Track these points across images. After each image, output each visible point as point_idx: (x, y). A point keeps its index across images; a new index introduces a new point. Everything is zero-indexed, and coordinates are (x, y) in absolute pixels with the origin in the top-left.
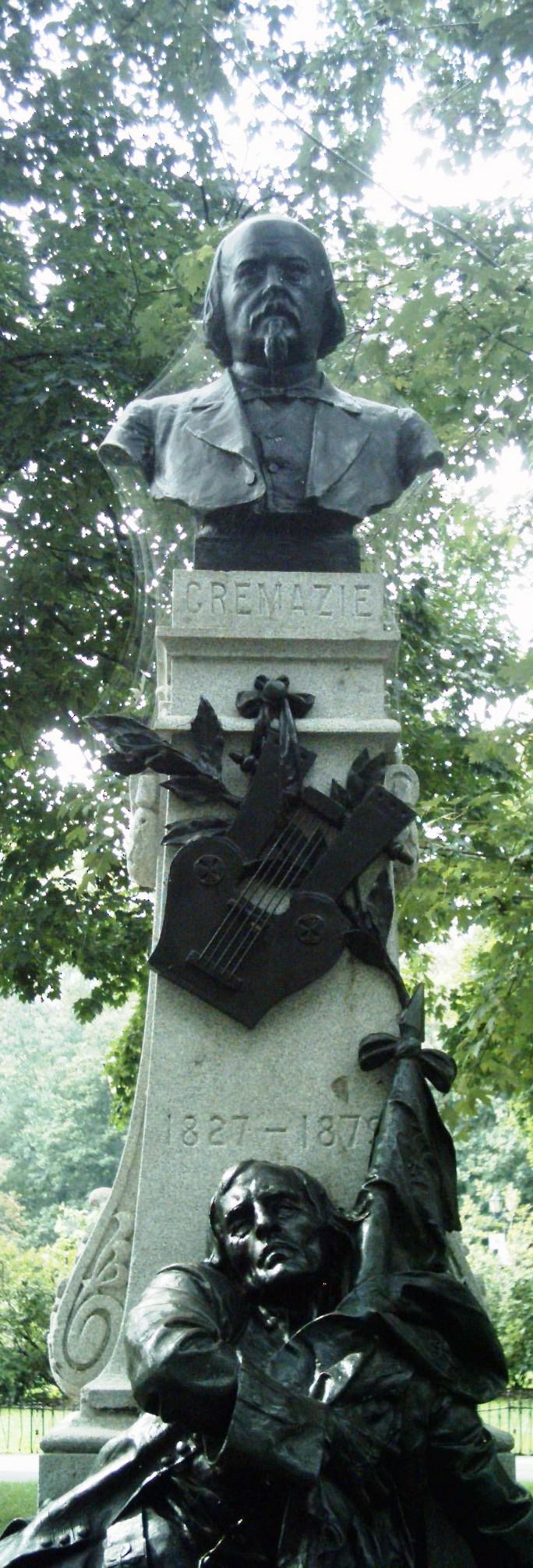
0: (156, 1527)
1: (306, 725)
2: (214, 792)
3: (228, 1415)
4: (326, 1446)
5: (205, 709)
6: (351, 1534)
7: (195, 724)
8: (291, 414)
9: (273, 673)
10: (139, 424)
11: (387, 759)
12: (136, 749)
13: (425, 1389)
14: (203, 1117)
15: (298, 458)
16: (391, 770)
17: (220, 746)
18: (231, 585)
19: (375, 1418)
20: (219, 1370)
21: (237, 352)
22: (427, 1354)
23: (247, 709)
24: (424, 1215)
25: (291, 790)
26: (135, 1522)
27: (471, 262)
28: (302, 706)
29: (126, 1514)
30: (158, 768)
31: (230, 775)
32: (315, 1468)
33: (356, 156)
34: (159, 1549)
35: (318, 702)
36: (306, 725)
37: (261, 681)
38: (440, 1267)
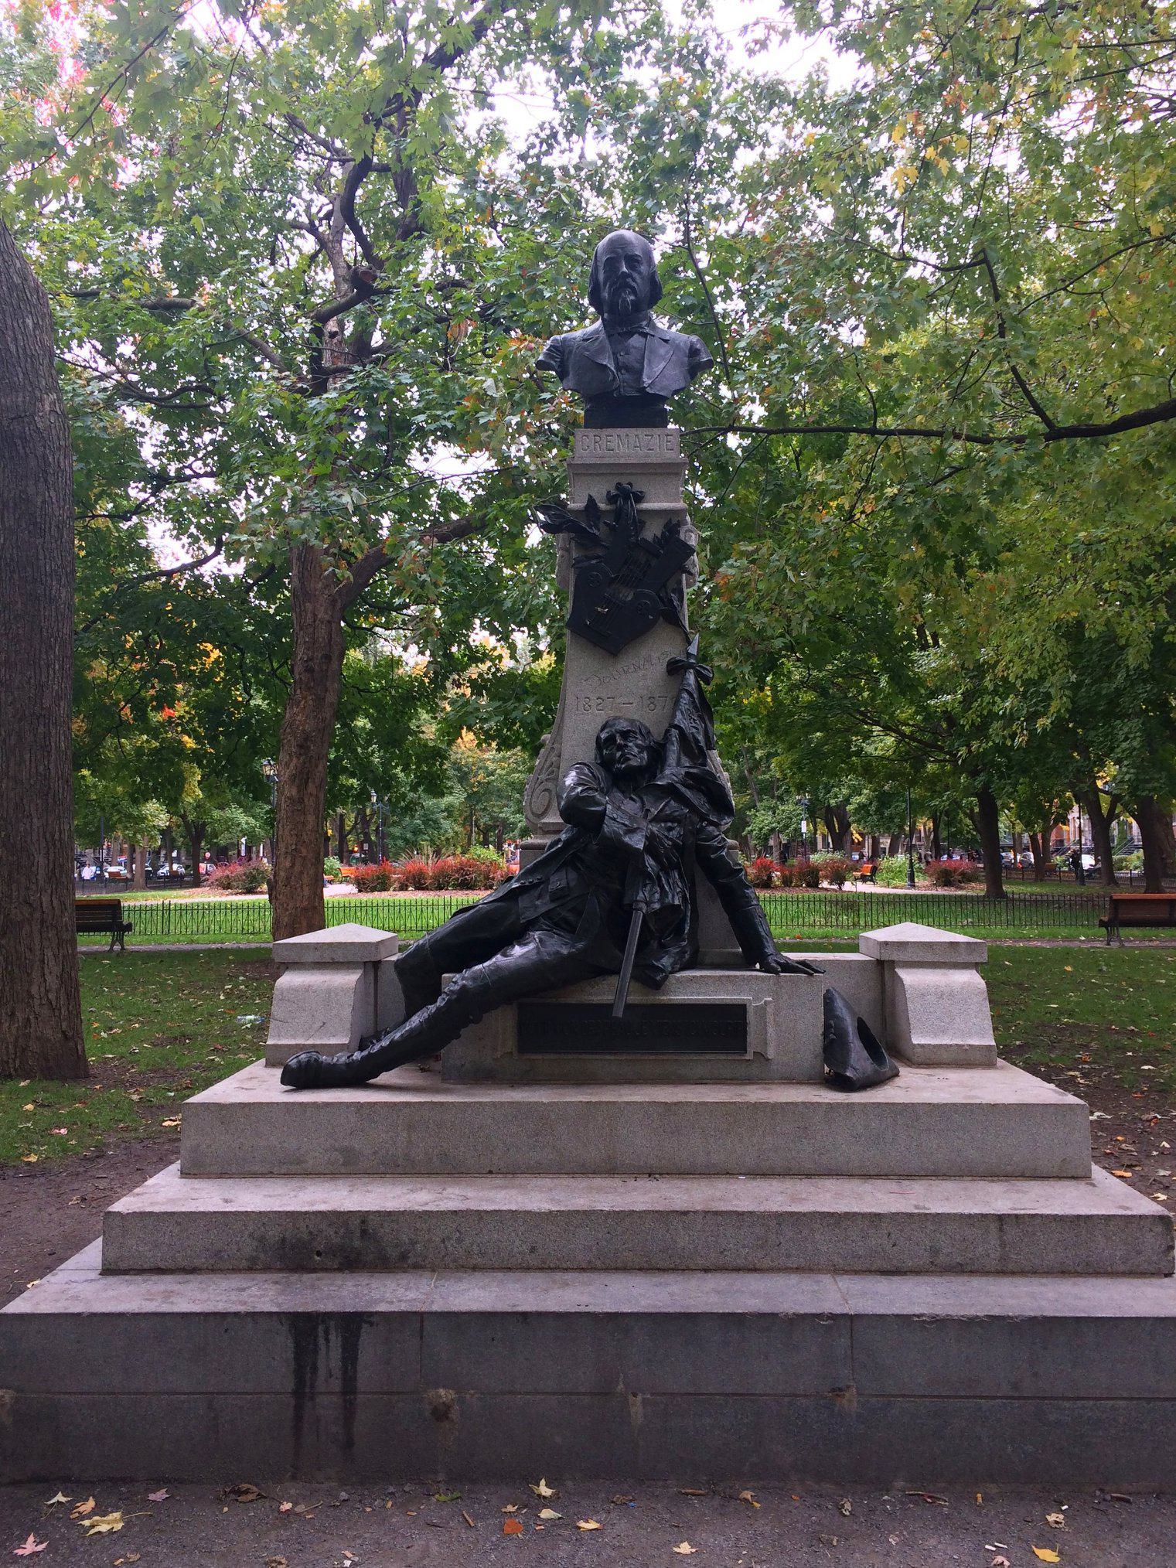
0: (573, 875)
1: (644, 506)
2: (595, 540)
3: (602, 821)
4: (647, 837)
5: (591, 500)
6: (660, 880)
7: (587, 507)
8: (636, 341)
9: (624, 481)
10: (562, 353)
11: (681, 523)
12: (559, 520)
13: (696, 819)
14: (593, 697)
15: (637, 365)
16: (685, 528)
17: (599, 518)
18: (603, 436)
19: (670, 829)
20: (598, 804)
21: (605, 308)
22: (696, 802)
23: (611, 499)
24: (697, 741)
25: (633, 539)
26: (563, 874)
27: (1058, 859)
28: (639, 498)
29: (558, 870)
30: (568, 530)
31: (601, 532)
32: (641, 846)
33: (865, 703)
34: (572, 884)
35: (647, 496)
36: (644, 506)
37: (619, 486)
38: (704, 764)
